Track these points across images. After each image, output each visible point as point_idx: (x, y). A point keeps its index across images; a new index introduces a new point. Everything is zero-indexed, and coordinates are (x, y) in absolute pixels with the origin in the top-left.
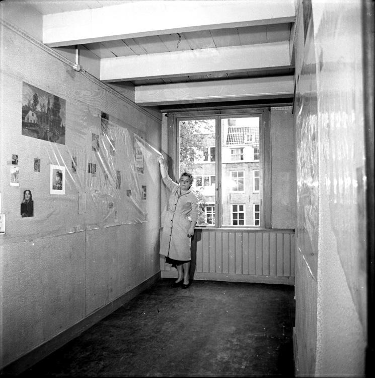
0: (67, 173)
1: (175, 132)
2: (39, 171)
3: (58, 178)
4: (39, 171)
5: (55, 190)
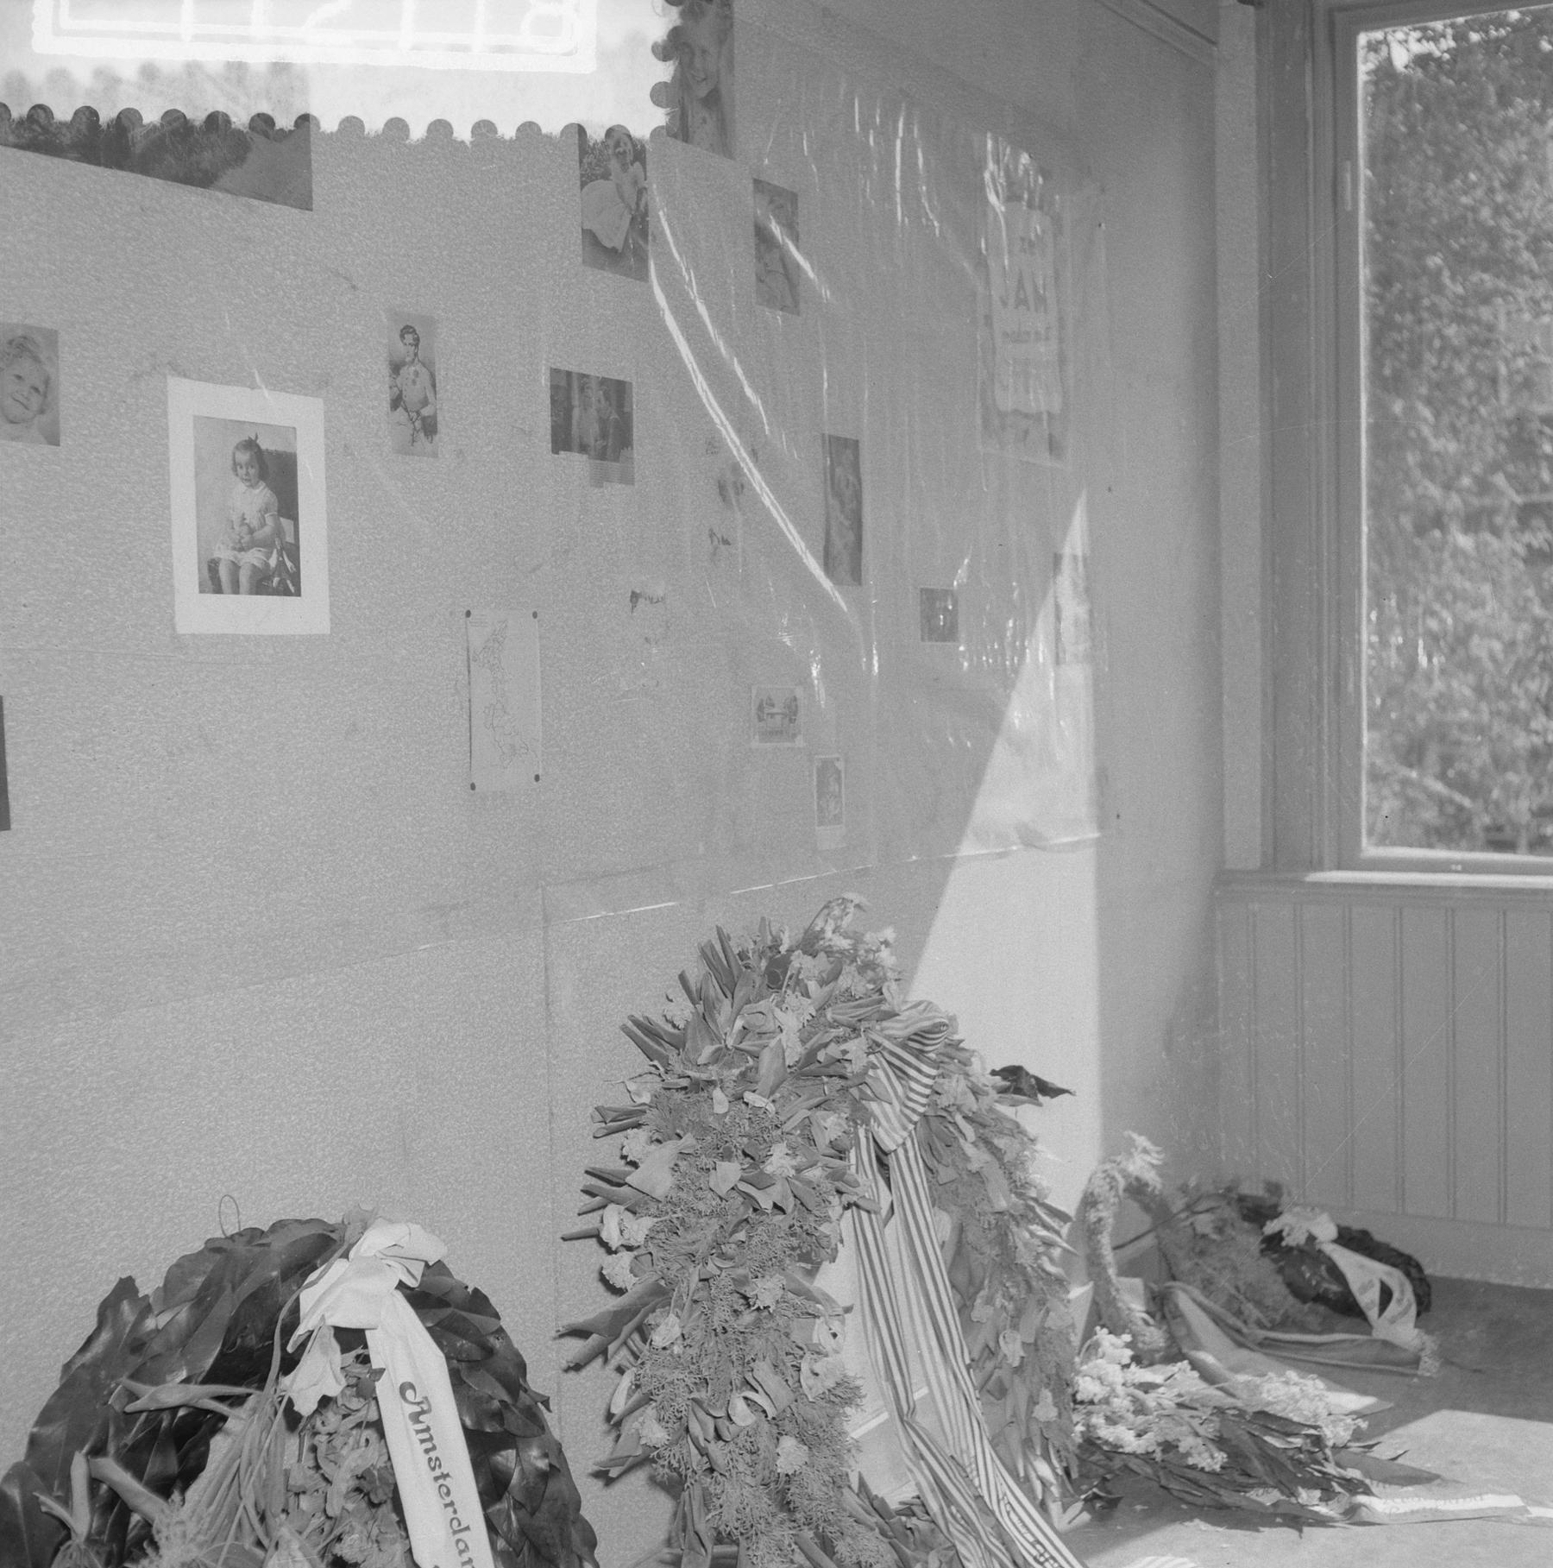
0: (339, 451)
1: (957, 1134)
2: (53, 440)
3: (252, 500)
4: (53, 440)
5: (227, 599)
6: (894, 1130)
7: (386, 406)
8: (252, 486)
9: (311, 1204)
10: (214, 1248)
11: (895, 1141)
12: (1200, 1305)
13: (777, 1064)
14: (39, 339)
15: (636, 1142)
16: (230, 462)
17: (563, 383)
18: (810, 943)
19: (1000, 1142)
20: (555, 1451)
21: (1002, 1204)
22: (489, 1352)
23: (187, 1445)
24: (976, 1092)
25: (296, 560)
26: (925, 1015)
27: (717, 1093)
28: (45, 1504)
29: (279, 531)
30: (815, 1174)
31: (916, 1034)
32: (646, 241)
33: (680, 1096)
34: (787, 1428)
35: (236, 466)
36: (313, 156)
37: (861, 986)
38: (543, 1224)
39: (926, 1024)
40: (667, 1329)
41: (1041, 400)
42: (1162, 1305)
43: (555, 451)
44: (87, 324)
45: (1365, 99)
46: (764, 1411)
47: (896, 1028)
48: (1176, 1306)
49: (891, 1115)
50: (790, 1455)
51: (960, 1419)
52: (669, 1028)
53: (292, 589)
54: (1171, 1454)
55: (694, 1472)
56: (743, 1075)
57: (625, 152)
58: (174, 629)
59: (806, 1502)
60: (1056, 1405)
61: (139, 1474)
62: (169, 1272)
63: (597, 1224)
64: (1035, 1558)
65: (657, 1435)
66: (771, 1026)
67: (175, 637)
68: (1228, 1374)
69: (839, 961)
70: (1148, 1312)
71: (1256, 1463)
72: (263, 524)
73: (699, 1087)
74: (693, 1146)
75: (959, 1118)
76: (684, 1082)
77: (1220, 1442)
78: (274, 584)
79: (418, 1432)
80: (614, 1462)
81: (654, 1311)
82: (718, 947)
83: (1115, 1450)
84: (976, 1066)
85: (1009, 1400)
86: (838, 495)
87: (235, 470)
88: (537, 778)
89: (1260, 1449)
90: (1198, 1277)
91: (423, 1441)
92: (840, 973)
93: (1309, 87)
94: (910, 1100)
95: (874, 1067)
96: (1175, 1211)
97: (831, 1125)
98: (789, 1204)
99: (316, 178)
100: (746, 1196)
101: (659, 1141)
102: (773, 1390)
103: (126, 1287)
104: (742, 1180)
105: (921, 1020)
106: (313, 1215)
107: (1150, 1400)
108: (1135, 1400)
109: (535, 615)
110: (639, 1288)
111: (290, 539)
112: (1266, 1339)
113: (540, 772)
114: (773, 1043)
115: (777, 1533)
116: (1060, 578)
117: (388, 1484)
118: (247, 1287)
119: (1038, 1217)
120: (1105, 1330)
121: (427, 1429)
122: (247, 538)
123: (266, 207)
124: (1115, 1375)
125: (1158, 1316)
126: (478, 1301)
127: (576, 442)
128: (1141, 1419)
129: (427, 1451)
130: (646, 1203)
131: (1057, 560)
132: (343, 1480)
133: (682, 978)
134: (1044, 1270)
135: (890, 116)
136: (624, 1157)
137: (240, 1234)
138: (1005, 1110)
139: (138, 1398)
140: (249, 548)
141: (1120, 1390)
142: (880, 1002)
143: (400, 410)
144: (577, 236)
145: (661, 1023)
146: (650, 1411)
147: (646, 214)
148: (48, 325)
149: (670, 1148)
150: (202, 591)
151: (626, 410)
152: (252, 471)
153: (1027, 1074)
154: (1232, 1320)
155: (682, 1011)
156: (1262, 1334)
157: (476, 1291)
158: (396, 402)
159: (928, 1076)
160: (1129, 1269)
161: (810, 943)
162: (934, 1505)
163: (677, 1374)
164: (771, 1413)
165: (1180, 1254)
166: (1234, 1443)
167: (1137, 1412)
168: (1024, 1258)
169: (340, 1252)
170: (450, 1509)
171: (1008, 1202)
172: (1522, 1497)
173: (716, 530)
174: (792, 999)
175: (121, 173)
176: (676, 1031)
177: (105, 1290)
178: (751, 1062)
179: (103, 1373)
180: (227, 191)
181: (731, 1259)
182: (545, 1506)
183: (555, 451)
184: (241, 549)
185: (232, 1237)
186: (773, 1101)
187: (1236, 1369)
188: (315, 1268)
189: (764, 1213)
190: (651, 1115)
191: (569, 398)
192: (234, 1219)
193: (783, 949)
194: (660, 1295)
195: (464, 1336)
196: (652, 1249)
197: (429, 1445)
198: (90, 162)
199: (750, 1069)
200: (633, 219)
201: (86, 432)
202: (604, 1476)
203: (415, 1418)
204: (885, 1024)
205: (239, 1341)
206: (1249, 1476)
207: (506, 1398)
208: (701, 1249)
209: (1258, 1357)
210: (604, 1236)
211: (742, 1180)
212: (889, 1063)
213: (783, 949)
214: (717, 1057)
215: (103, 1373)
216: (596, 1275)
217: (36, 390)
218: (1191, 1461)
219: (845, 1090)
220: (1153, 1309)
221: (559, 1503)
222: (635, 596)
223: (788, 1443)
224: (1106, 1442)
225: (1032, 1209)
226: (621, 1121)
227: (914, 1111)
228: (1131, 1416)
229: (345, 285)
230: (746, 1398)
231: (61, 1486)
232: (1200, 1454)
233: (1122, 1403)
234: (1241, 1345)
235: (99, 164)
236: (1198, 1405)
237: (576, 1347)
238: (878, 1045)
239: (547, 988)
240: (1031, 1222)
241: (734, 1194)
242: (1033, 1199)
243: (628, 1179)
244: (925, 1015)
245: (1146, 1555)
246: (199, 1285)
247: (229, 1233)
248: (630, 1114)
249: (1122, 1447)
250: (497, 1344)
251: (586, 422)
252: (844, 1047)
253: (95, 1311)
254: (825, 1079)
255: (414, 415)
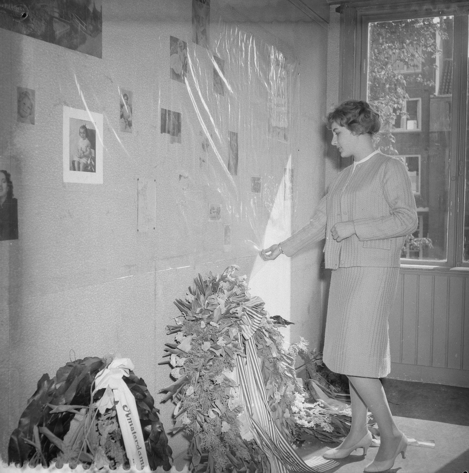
0: (107, 130)
3: (83, 143)
5: (77, 173)
6: (249, 334)
7: (119, 117)
8: (84, 139)
9: (93, 353)
10: (69, 365)
11: (249, 337)
12: (318, 385)
13: (219, 314)
14: (30, 93)
15: (179, 336)
16: (79, 132)
17: (164, 113)
18: (223, 278)
19: (275, 337)
20: (161, 426)
21: (275, 355)
22: (145, 396)
23: (65, 423)
24: (269, 323)
25: (95, 162)
26: (257, 300)
27: (202, 322)
28: (25, 441)
29: (91, 153)
30: (230, 345)
31: (255, 306)
32: (186, 72)
33: (191, 323)
34: (224, 419)
35: (80, 132)
36: (103, 43)
37: (239, 292)
38: (152, 360)
39: (259, 303)
40: (190, 390)
41: (283, 124)
42: (308, 385)
43: (162, 133)
44: (43, 89)
45: (370, 42)
46: (218, 414)
47: (249, 304)
48: (312, 386)
49: (248, 329)
50: (225, 427)
51: (264, 417)
52: (187, 303)
53: (93, 170)
54: (318, 428)
55: (197, 432)
56: (209, 317)
57: (182, 46)
58: (63, 181)
59: (229, 440)
60: (290, 413)
61: (52, 431)
62: (57, 372)
63: (169, 360)
64: (286, 457)
65: (187, 421)
66: (216, 303)
67: (63, 183)
68: (329, 406)
69: (233, 284)
70: (304, 388)
71: (342, 430)
72: (87, 151)
73: (197, 320)
74: (196, 337)
75: (264, 330)
76: (194, 318)
77: (332, 424)
78: (89, 169)
79: (128, 420)
80: (175, 429)
81: (185, 385)
82: (199, 279)
83: (302, 426)
84: (268, 316)
85: (277, 412)
86: (232, 149)
87: (80, 134)
88: (154, 228)
89: (343, 426)
90: (317, 378)
91: (129, 422)
92: (233, 288)
93: (355, 37)
94: (254, 324)
95: (244, 315)
96: (311, 359)
97: (234, 331)
98: (224, 354)
99: (103, 49)
100: (212, 352)
101: (186, 336)
102: (221, 408)
103: (45, 377)
104: (211, 347)
105: (256, 302)
106: (96, 356)
107: (311, 412)
108: (307, 412)
109: (155, 181)
110: (181, 378)
111: (93, 155)
112: (337, 395)
113: (155, 227)
114: (217, 307)
115: (221, 449)
116: (286, 176)
117: (119, 435)
118: (81, 377)
119: (284, 359)
120: (297, 393)
121: (130, 419)
122: (82, 155)
123: (90, 57)
124: (301, 406)
125: (307, 389)
126: (141, 381)
127: (167, 130)
128: (309, 418)
129: (130, 425)
130: (182, 354)
131: (285, 169)
132: (105, 435)
133: (190, 289)
134: (286, 375)
135: (248, 38)
136: (176, 341)
137: (76, 361)
138: (275, 329)
139: (52, 410)
140: (83, 157)
141: (303, 410)
142: (244, 296)
143: (123, 118)
144: (169, 70)
145: (185, 301)
146: (185, 414)
147: (186, 64)
148: (32, 89)
149: (190, 338)
150: (70, 170)
151: (180, 121)
152: (84, 135)
153: (282, 318)
154: (327, 390)
155: (191, 298)
156: (336, 394)
157: (141, 378)
158: (122, 116)
159: (260, 318)
160: (299, 376)
161: (223, 278)
162: (259, 442)
163: (193, 404)
164: (220, 415)
165: (312, 371)
166: (336, 424)
167: (307, 416)
168: (281, 371)
169: (106, 367)
170: (137, 442)
171: (277, 355)
172: (415, 439)
173: (201, 158)
174: (221, 295)
175: (53, 44)
176: (189, 304)
177: (40, 377)
178: (211, 313)
179: (40, 402)
180: (80, 51)
181: (208, 370)
182: (159, 442)
183: (162, 133)
184: (81, 158)
185: (74, 362)
186: (219, 324)
187: (330, 404)
188: (98, 372)
189: (217, 357)
190: (183, 328)
191: (165, 117)
192: (73, 357)
193: (217, 280)
194: (187, 381)
195: (138, 392)
196: (184, 367)
197: (131, 424)
198: (45, 41)
199: (211, 315)
200: (183, 66)
201: (41, 121)
202: (172, 434)
203: (127, 415)
204: (246, 303)
205: (80, 392)
206: (340, 434)
207: (150, 410)
208: (199, 367)
209: (336, 401)
210: (171, 363)
211: (211, 347)
212: (247, 313)
213: (217, 280)
214: (201, 312)
215: (40, 402)
216: (169, 376)
217: (29, 108)
218: (324, 430)
219: (236, 321)
220: (305, 387)
221: (163, 441)
222: (180, 176)
223: (225, 423)
224: (299, 424)
225: (282, 357)
226: (174, 330)
227: (255, 328)
228: (305, 417)
229: (110, 81)
230: (213, 410)
231: (29, 436)
232: (326, 427)
233: (303, 413)
234: (330, 397)
235: (47, 41)
236: (326, 414)
237: (164, 396)
238: (245, 309)
239: (155, 290)
240: (282, 361)
241: (208, 351)
242: (283, 354)
243: (178, 347)
244: (257, 300)
245: (314, 456)
246: (67, 376)
247: (73, 361)
248: (176, 328)
249: (304, 426)
250: (146, 394)
251: (170, 125)
252: (236, 309)
253: (37, 384)
254: (231, 318)
255: (126, 120)
